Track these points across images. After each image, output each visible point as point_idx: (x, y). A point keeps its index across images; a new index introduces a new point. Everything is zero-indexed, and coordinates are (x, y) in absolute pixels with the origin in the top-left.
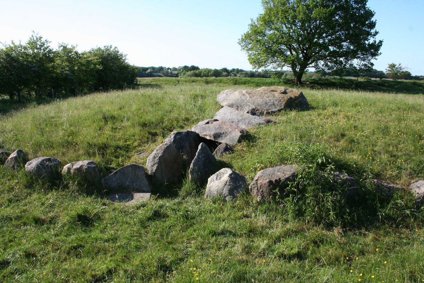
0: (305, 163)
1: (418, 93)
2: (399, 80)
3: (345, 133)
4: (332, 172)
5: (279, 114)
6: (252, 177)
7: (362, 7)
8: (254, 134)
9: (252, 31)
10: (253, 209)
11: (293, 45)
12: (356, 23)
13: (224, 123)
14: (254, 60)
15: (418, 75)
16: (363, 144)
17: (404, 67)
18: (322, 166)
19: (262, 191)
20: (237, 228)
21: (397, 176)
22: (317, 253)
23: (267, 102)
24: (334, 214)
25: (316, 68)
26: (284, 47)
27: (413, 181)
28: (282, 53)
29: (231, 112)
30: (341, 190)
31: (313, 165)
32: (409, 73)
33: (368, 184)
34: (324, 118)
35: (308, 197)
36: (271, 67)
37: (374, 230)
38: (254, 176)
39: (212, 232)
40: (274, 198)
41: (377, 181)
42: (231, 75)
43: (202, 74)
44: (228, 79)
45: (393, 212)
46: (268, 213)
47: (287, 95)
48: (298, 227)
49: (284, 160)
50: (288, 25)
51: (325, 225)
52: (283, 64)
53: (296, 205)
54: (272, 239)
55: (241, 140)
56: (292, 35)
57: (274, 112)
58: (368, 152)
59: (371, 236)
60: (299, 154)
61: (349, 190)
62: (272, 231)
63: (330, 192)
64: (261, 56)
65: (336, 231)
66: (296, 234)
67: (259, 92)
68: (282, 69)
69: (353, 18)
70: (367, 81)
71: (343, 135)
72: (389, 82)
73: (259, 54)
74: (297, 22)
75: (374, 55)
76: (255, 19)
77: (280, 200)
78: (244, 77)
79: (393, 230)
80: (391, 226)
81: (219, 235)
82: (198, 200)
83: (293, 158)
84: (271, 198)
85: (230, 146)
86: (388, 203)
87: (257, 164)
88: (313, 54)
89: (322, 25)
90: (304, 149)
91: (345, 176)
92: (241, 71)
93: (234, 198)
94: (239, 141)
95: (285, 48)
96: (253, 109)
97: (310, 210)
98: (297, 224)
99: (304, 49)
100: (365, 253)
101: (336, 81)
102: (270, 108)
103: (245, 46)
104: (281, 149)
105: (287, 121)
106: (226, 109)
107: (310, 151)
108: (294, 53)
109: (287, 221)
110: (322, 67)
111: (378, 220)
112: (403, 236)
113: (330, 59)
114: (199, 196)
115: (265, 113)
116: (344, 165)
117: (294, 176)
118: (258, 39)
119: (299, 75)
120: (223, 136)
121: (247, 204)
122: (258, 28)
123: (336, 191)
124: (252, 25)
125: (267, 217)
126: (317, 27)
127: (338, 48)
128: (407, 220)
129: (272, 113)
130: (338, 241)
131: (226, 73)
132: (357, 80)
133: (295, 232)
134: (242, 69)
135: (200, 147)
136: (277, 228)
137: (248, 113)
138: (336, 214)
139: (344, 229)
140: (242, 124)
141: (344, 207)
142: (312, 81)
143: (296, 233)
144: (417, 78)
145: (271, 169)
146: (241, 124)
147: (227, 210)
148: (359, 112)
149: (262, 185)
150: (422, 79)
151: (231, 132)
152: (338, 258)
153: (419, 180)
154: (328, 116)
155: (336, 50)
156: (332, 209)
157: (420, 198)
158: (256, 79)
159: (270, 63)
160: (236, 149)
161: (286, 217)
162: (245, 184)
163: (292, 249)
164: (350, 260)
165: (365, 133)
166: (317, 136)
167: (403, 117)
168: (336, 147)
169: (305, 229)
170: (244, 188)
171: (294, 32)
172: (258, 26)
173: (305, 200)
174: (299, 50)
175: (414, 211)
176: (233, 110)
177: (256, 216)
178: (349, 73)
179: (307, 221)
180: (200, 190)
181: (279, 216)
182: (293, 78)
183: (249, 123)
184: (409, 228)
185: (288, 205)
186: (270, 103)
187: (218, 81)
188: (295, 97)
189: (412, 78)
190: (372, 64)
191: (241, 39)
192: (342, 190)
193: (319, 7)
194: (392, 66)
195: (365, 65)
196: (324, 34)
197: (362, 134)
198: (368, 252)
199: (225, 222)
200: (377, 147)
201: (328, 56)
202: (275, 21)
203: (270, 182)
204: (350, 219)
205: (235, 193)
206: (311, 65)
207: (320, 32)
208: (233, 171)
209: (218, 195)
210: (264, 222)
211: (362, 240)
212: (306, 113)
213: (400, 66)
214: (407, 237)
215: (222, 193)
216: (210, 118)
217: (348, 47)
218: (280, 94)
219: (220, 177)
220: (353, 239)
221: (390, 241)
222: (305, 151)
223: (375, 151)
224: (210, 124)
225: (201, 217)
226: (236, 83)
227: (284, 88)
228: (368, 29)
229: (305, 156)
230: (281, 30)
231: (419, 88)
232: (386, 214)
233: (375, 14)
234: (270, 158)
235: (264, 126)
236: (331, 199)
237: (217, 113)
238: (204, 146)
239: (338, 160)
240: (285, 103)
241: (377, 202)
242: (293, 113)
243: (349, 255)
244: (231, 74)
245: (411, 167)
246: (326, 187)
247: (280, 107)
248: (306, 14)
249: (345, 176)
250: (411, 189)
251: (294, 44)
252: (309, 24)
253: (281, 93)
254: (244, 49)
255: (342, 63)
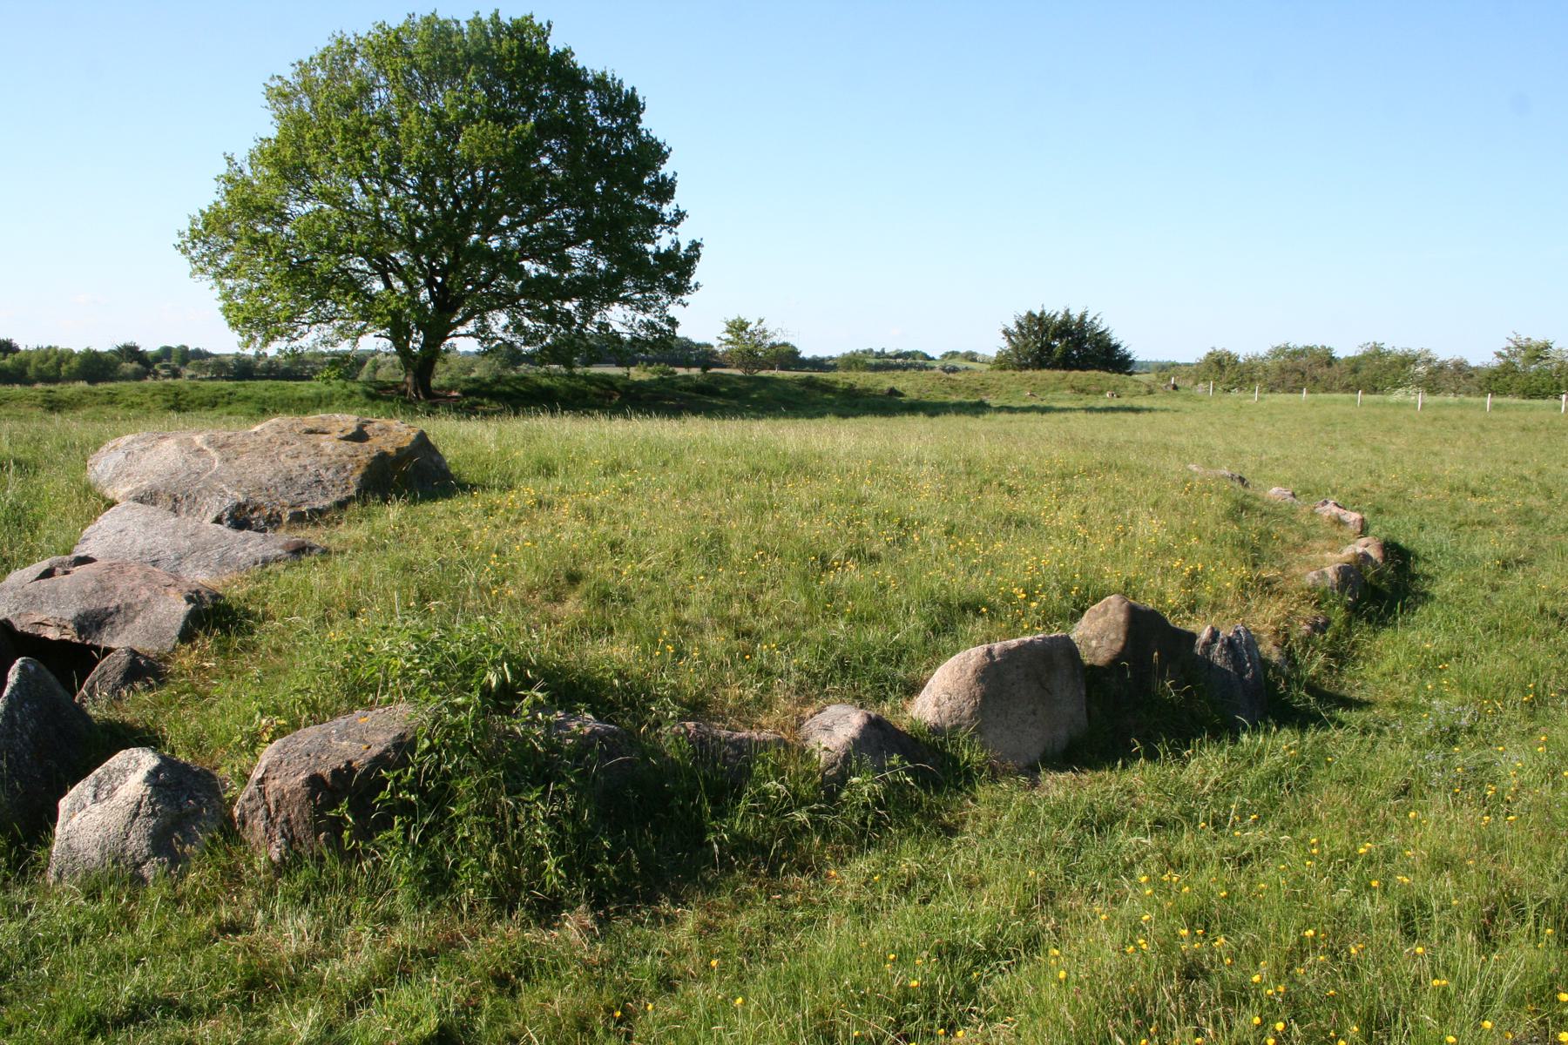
0: (440, 693)
1: (821, 415)
2: (763, 373)
3: (581, 568)
4: (540, 715)
5: (340, 518)
6: (241, 771)
7: (628, 127)
8: (243, 604)
9: (233, 202)
10: (256, 896)
11: (393, 255)
12: (612, 181)
13: (117, 568)
14: (246, 314)
15: (822, 352)
16: (642, 604)
17: (773, 330)
18: (503, 699)
19: (287, 821)
20: (197, 978)
21: (758, 699)
22: (510, 1017)
23: (294, 474)
24: (558, 866)
25: (483, 340)
26: (361, 263)
27: (811, 710)
28: (352, 286)
29: (146, 525)
30: (576, 776)
31: (470, 698)
32: (793, 347)
33: (667, 740)
34: (507, 520)
35: (460, 818)
36: (311, 339)
37: (700, 898)
38: (251, 767)
39: (89, 1021)
40: (333, 839)
41: (697, 726)
42: (156, 373)
43: (31, 372)
44: (145, 390)
45: (756, 823)
46: (317, 899)
47: (370, 442)
48: (435, 933)
49: (363, 689)
50: (371, 181)
51: (533, 908)
52: (358, 326)
53: (418, 852)
54: (340, 998)
55: (192, 630)
56: (388, 219)
57: (321, 512)
58: (660, 629)
59: (691, 919)
60: (417, 661)
61: (606, 771)
62: (338, 966)
63: (538, 786)
64: (271, 297)
65: (574, 925)
66: (431, 962)
67: (258, 438)
68: (354, 344)
69: (601, 162)
70: (662, 379)
71: (574, 579)
72: (728, 380)
73: (264, 290)
74: (402, 171)
75: (677, 289)
76: (241, 157)
77: (357, 844)
78: (211, 379)
79: (760, 886)
80: (754, 873)
81: (118, 1023)
82: (20, 895)
83: (394, 681)
84: (325, 839)
85: (147, 658)
86: (738, 798)
87: (257, 717)
88: (470, 287)
89: (494, 185)
90: (433, 642)
91: (586, 723)
92: (199, 355)
93: (173, 863)
94: (186, 635)
95: (365, 266)
96: (239, 505)
97: (472, 866)
98: (432, 924)
99: (434, 272)
100: (677, 982)
101: (556, 383)
102: (304, 497)
103: (206, 259)
104: (350, 651)
105: (370, 541)
106: (126, 513)
107: (456, 647)
108: (398, 284)
109: (391, 919)
110: (503, 336)
111: (708, 859)
112: (791, 899)
113: (528, 306)
114: (21, 881)
115: (286, 518)
116: (581, 686)
117: (403, 746)
118: (256, 231)
119: (422, 366)
120: (119, 619)
121: (233, 877)
122: (254, 193)
123: (561, 779)
124: (230, 180)
125: (314, 915)
126: (475, 194)
127: (555, 268)
128: (803, 843)
129: (316, 516)
130: (581, 959)
131: (135, 365)
132: (627, 378)
133: (426, 954)
134: (202, 347)
135: (16, 676)
136: (354, 952)
137: (218, 520)
138: (568, 865)
139: (601, 913)
140: (197, 566)
141: (592, 834)
142: (472, 386)
143: (429, 956)
144: (818, 364)
145: (313, 730)
146: (190, 566)
147: (150, 917)
148: (626, 491)
149: (283, 796)
150: (834, 368)
151: (148, 601)
152: (586, 1019)
153: (829, 704)
154: (520, 514)
155: (548, 275)
156: (551, 846)
157: (835, 764)
158: (259, 387)
159: (309, 325)
160: (172, 668)
161: (387, 904)
162: (217, 803)
163: (416, 1021)
164: (627, 1017)
165: (650, 562)
166: (482, 589)
167: (770, 497)
168: (551, 621)
169: (460, 939)
170: (213, 820)
171: (393, 208)
172: (255, 182)
173: (452, 831)
174: (417, 274)
175: (821, 811)
176: (160, 516)
177: (272, 917)
178: (595, 357)
179: (465, 907)
180: (24, 854)
181: (360, 904)
182: (402, 378)
183: (223, 562)
184: (810, 870)
185: (391, 857)
186: (303, 480)
187: (99, 399)
188: (398, 449)
189: (889, 357)
190: (673, 322)
191: (187, 233)
192: (578, 776)
193: (482, 122)
194: (738, 327)
195: (650, 326)
196: (505, 217)
197: (640, 566)
198: (685, 977)
199: (144, 968)
200: (691, 609)
201: (522, 296)
202: (321, 166)
203: (315, 781)
204: (615, 872)
205: (178, 842)
206: (461, 330)
207: (488, 211)
208: (163, 758)
209: (109, 861)
210: (303, 939)
211: (662, 939)
212: (440, 506)
213: (760, 328)
214: (807, 901)
215: (123, 850)
216: (57, 553)
217: (587, 263)
218: (343, 443)
219: (108, 787)
220: (633, 942)
221: (754, 925)
222: (439, 650)
223: (686, 623)
224: (58, 578)
225: (37, 965)
226: (178, 404)
227: (355, 418)
228: (652, 201)
229: (438, 670)
230: (344, 201)
231: (826, 396)
232: (734, 837)
233: (671, 154)
234: (307, 690)
235: (281, 566)
236: (544, 814)
237: (88, 530)
238: (32, 668)
239: (560, 669)
240: (363, 475)
241: (701, 801)
242: (394, 512)
243: (622, 1004)
244: (156, 367)
245: (800, 664)
246: (524, 773)
247: (343, 491)
248: (434, 145)
249: (586, 723)
250: (805, 740)
251: (397, 251)
252: (446, 181)
253: (347, 438)
254: (202, 270)
255: (572, 322)
